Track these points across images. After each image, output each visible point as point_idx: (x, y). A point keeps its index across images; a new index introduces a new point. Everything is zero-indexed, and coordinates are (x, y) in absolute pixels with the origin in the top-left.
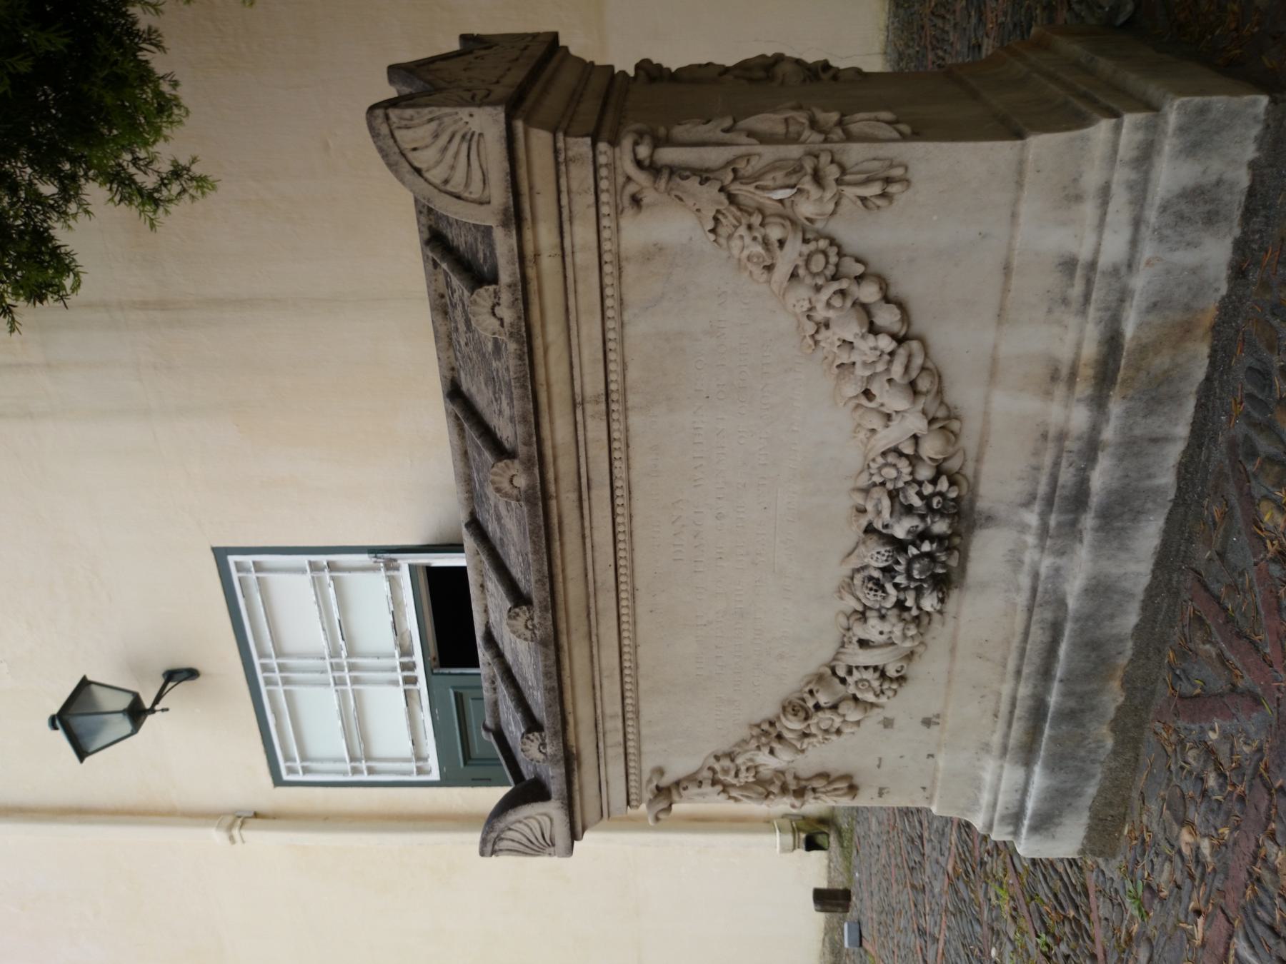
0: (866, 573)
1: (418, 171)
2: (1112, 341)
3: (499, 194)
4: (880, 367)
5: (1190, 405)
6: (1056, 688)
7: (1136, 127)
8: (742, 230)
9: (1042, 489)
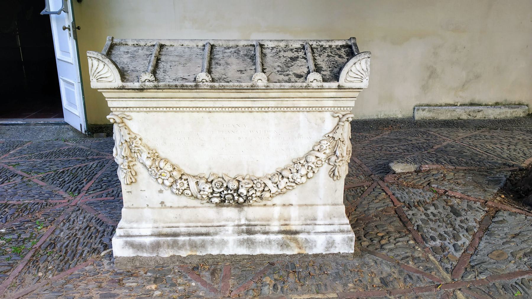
0: (223, 182)
1: (355, 64)
2: (296, 233)
3: (347, 85)
4: (291, 180)
5: (281, 253)
6: (187, 238)
7: (348, 228)
8: (329, 144)
9: (252, 223)
